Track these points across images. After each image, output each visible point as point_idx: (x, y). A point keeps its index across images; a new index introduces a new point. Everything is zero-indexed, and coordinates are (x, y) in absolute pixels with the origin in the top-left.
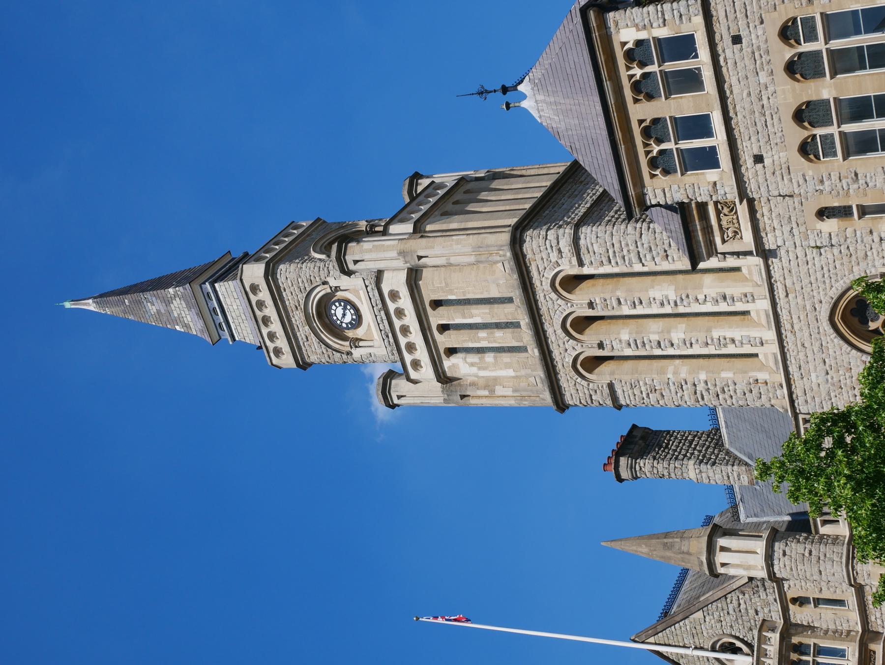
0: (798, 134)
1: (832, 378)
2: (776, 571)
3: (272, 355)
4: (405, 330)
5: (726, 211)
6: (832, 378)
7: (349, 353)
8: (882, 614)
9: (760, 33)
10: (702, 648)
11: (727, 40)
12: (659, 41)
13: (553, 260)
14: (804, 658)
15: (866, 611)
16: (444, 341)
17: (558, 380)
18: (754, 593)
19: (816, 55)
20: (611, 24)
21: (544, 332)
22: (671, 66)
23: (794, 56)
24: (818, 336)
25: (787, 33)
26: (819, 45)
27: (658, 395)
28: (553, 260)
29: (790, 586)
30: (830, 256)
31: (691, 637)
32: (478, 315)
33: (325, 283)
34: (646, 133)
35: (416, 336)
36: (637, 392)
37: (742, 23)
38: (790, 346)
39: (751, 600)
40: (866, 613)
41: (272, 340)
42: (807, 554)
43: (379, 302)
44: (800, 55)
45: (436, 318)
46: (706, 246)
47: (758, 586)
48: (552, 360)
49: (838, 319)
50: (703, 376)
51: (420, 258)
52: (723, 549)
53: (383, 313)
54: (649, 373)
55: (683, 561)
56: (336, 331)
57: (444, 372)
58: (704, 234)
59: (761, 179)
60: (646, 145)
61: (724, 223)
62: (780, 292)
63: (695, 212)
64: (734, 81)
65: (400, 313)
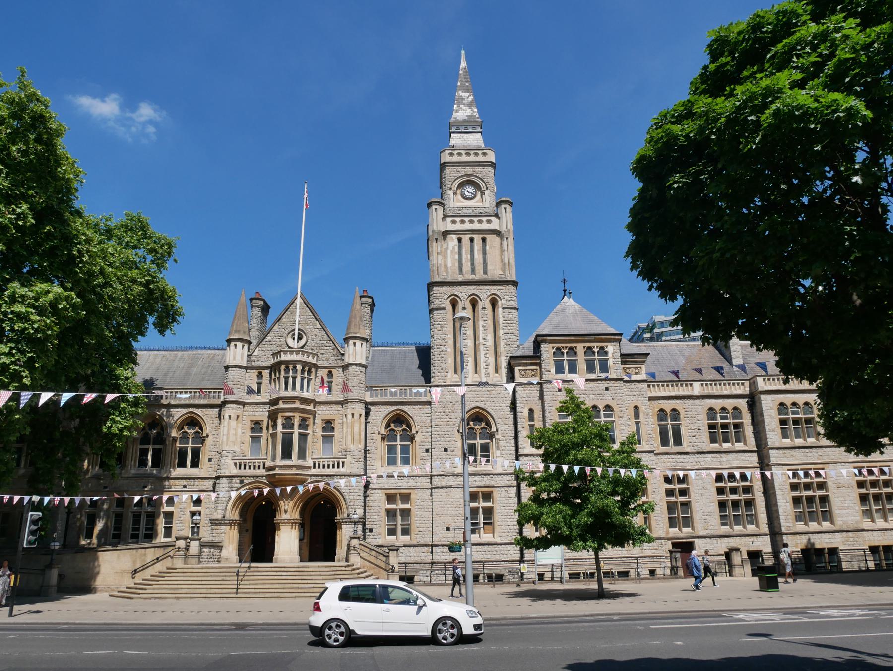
3: (450, 151)
4: (480, 222)
5: (534, 373)
7: (451, 189)
9: (609, 398)
11: (607, 386)
12: (607, 360)
13: (505, 297)
16: (466, 238)
17: (446, 285)
19: (288, 373)
20: (615, 343)
21: (471, 285)
22: (597, 363)
23: (599, 408)
25: (608, 407)
27: (439, 329)
28: (505, 297)
30: (506, 410)
31: (304, 320)
32: (478, 257)
33: (487, 189)
34: (571, 348)
36: (441, 320)
37: (613, 392)
41: (458, 153)
42: (361, 382)
44: (599, 411)
45: (477, 238)
48: (457, 285)
50: (449, 350)
51: (507, 238)
54: (470, 332)
55: (355, 325)
56: (461, 185)
57: (450, 234)
58: (524, 363)
59: (551, 389)
60: (566, 347)
61: (528, 372)
64: (591, 385)
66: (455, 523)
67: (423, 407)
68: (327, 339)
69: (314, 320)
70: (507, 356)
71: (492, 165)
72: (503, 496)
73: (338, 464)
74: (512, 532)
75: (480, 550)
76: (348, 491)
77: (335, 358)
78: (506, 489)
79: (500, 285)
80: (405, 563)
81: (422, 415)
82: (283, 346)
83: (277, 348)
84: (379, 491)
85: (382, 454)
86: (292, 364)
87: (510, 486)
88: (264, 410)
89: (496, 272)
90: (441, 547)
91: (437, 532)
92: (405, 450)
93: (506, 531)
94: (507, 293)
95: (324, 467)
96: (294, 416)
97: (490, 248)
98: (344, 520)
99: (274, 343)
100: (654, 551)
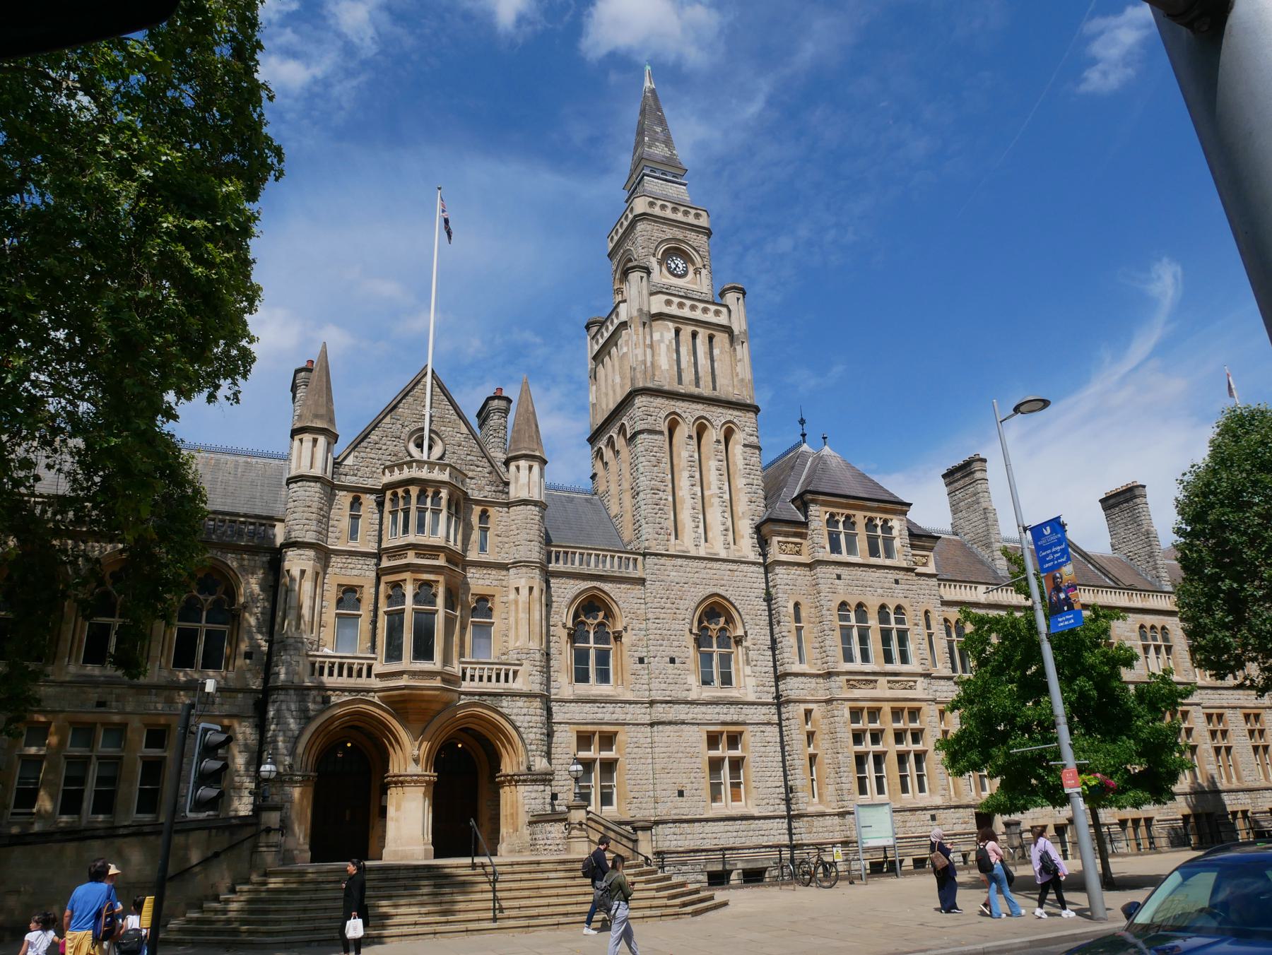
0: (853, 604)
2: (529, 507)
3: (651, 199)
4: (693, 308)
5: (798, 549)
10: (431, 421)
11: (898, 577)
13: (746, 428)
14: (429, 500)
15: (481, 567)
16: (687, 330)
17: (663, 397)
21: (698, 403)
26: (893, 624)
27: (655, 463)
34: (848, 517)
35: (698, 315)
38: (695, 563)
43: (691, 296)
45: (703, 334)
46: (779, 531)
47: (497, 486)
48: (678, 400)
49: (717, 599)
52: (530, 468)
53: (683, 294)
55: (529, 437)
60: (842, 514)
61: (790, 545)
62: (732, 566)
64: (877, 575)
65: (705, 310)
66: (692, 783)
67: (633, 587)
68: (478, 454)
69: (456, 417)
70: (753, 520)
71: (708, 232)
72: (758, 739)
73: (498, 676)
74: (774, 799)
75: (730, 828)
76: (526, 725)
77: (493, 488)
78: (763, 728)
80: (721, 850)
81: (631, 599)
82: (400, 455)
83: (389, 458)
84: (567, 727)
85: (569, 662)
86: (432, 487)
87: (768, 724)
88: (365, 567)
89: (727, 389)
90: (671, 825)
91: (665, 799)
92: (603, 658)
93: (765, 796)
95: (481, 679)
96: (438, 581)
97: (721, 352)
98: (522, 778)
99: (384, 447)
100: (964, 825)
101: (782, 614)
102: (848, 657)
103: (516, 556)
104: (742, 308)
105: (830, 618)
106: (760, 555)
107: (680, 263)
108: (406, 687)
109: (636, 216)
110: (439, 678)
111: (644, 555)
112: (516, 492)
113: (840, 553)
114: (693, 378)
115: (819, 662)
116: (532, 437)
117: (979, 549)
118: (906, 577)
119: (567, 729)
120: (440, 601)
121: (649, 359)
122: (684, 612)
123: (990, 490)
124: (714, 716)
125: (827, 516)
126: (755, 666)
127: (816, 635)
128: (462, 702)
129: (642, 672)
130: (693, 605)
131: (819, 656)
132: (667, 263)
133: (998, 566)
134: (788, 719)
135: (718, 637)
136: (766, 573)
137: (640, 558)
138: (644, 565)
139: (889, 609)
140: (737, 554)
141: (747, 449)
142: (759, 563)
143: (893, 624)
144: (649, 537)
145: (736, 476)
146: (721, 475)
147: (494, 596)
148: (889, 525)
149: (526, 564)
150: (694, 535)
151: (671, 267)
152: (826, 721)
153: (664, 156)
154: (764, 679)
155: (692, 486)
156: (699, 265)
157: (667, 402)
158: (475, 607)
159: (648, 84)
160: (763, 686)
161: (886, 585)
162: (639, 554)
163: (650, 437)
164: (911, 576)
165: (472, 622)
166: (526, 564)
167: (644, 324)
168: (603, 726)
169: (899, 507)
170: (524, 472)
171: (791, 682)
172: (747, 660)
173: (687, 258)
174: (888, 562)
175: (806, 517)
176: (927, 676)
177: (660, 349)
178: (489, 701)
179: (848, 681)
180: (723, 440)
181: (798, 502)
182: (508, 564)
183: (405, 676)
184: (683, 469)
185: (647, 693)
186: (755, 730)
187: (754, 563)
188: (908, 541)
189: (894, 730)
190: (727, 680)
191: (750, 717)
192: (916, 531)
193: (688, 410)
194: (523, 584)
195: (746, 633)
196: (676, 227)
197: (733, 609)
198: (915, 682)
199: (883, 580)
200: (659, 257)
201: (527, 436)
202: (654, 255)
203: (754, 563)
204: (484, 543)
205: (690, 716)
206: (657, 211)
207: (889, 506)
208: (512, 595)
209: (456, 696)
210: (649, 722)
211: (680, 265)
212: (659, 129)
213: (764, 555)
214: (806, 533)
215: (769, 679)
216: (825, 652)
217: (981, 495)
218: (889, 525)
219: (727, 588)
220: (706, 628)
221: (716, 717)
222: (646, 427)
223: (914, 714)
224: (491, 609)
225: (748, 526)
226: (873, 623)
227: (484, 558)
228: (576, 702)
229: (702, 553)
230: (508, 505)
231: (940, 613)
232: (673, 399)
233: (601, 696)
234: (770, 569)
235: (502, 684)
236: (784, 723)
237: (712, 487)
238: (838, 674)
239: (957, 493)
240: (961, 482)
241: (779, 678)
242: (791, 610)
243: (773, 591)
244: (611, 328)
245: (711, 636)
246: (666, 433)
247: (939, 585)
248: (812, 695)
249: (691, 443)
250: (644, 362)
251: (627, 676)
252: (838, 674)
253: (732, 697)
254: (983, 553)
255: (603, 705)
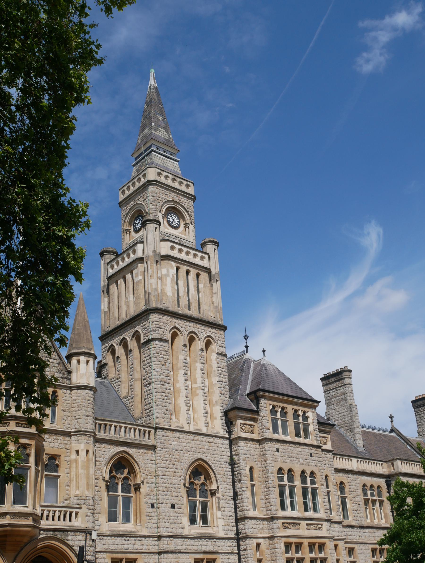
1: (174, 452)
3: (159, 171)
5: (252, 429)
6: (174, 452)
8: (50, 442)
11: (311, 452)
13: (219, 342)
15: (52, 433)
16: (184, 269)
17: (168, 315)
18: (59, 370)
21: (190, 321)
24: (193, 451)
26: (309, 485)
29: (66, 393)
34: (283, 408)
35: (190, 258)
38: (188, 436)
39: (54, 366)
40: (50, 433)
45: (193, 272)
47: (63, 374)
48: (178, 318)
49: (200, 462)
52: (88, 362)
60: (280, 406)
63: (254, 416)
65: (195, 256)
67: (148, 452)
70: (222, 407)
78: (228, 556)
79: (214, 328)
81: (146, 461)
84: (104, 555)
87: (232, 553)
92: (127, 502)
94: (220, 339)
96: (31, 445)
101: (243, 475)
102: (283, 507)
103: (77, 427)
104: (217, 256)
105: (273, 479)
106: (227, 432)
107: (175, 218)
108: (9, 525)
109: (148, 181)
110: (31, 518)
111: (156, 429)
112: (76, 379)
113: (278, 433)
114: (187, 303)
115: (265, 509)
116: (89, 339)
117: (345, 432)
118: (316, 452)
119: (105, 556)
120: (32, 459)
121: (160, 287)
122: (180, 471)
123: (354, 392)
124: (199, 547)
125: (271, 407)
126: (224, 511)
127: (263, 490)
128: (41, 536)
129: (153, 514)
130: (186, 466)
131: (264, 505)
132: (167, 218)
133: (358, 445)
134: (245, 550)
135: (200, 490)
136: (231, 445)
137: (153, 431)
138: (155, 436)
139: (307, 473)
140: (214, 431)
141: (219, 357)
142: (226, 438)
143: (309, 485)
144: (158, 416)
145: (212, 375)
146: (203, 374)
147: (60, 456)
148: (306, 415)
149: (85, 433)
150: (187, 416)
151: (170, 221)
152: (269, 551)
153: (164, 139)
154: (229, 521)
155: (186, 380)
156: (188, 221)
157: (171, 319)
158: (47, 464)
159: (152, 82)
160: (229, 525)
161: (305, 457)
162: (152, 428)
163: (161, 343)
164: (319, 451)
165: (46, 475)
166: (85, 433)
167: (157, 262)
168: (128, 554)
169: (313, 403)
170: (83, 365)
171: (249, 524)
172: (219, 507)
173: (181, 216)
174: (306, 441)
175: (258, 408)
176: (328, 521)
177: (166, 281)
178: (59, 535)
179: (283, 523)
180: (205, 349)
181: (253, 396)
182: (70, 432)
183: (8, 516)
184: (180, 368)
185: (156, 530)
186: (224, 557)
187: (223, 438)
188: (317, 427)
189: (311, 558)
190: (205, 521)
191: (220, 548)
192: (321, 421)
193: (184, 326)
194: (82, 447)
195: (218, 487)
196: (174, 192)
197: (210, 470)
198: (322, 525)
199: (303, 453)
200: (163, 213)
201: (85, 338)
202: (160, 211)
203: (223, 438)
204: (53, 416)
205: (184, 547)
206: (162, 179)
207: (307, 402)
208: (74, 456)
209: (38, 531)
210: (157, 551)
211: (175, 220)
212: (161, 118)
213: (230, 432)
214: (257, 419)
215: (232, 521)
216: (269, 502)
217: (348, 395)
218: (306, 415)
219: (207, 455)
220: (115, 477)
221: (200, 548)
222: (158, 336)
223: (322, 547)
224: (57, 466)
225: (220, 411)
226: (298, 483)
227: (54, 427)
228: (111, 536)
229: (192, 429)
230: (71, 388)
231: (334, 477)
232: (174, 317)
233: (127, 531)
234: (234, 442)
235: (67, 522)
236: (242, 553)
237: (198, 382)
238: (278, 518)
239: (331, 391)
240: (334, 385)
241: (238, 520)
242: (248, 472)
243: (236, 458)
244: (127, 261)
245: (195, 489)
246: (170, 341)
247: (334, 457)
248: (261, 533)
249: (185, 350)
250: (156, 289)
251: (144, 517)
252: (278, 518)
253: (209, 534)
254: (348, 435)
255: (128, 538)
